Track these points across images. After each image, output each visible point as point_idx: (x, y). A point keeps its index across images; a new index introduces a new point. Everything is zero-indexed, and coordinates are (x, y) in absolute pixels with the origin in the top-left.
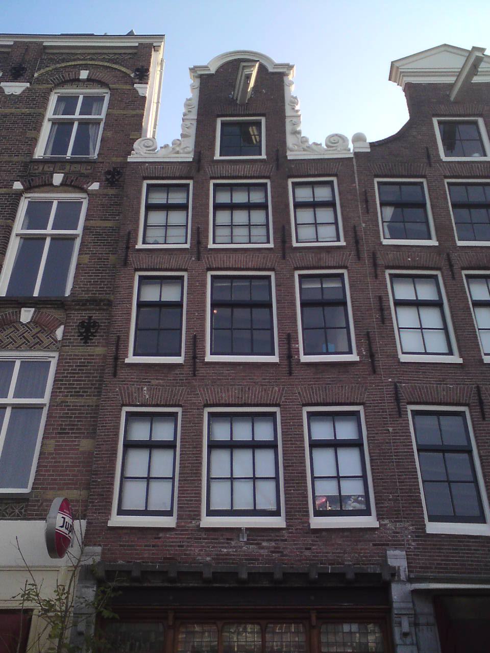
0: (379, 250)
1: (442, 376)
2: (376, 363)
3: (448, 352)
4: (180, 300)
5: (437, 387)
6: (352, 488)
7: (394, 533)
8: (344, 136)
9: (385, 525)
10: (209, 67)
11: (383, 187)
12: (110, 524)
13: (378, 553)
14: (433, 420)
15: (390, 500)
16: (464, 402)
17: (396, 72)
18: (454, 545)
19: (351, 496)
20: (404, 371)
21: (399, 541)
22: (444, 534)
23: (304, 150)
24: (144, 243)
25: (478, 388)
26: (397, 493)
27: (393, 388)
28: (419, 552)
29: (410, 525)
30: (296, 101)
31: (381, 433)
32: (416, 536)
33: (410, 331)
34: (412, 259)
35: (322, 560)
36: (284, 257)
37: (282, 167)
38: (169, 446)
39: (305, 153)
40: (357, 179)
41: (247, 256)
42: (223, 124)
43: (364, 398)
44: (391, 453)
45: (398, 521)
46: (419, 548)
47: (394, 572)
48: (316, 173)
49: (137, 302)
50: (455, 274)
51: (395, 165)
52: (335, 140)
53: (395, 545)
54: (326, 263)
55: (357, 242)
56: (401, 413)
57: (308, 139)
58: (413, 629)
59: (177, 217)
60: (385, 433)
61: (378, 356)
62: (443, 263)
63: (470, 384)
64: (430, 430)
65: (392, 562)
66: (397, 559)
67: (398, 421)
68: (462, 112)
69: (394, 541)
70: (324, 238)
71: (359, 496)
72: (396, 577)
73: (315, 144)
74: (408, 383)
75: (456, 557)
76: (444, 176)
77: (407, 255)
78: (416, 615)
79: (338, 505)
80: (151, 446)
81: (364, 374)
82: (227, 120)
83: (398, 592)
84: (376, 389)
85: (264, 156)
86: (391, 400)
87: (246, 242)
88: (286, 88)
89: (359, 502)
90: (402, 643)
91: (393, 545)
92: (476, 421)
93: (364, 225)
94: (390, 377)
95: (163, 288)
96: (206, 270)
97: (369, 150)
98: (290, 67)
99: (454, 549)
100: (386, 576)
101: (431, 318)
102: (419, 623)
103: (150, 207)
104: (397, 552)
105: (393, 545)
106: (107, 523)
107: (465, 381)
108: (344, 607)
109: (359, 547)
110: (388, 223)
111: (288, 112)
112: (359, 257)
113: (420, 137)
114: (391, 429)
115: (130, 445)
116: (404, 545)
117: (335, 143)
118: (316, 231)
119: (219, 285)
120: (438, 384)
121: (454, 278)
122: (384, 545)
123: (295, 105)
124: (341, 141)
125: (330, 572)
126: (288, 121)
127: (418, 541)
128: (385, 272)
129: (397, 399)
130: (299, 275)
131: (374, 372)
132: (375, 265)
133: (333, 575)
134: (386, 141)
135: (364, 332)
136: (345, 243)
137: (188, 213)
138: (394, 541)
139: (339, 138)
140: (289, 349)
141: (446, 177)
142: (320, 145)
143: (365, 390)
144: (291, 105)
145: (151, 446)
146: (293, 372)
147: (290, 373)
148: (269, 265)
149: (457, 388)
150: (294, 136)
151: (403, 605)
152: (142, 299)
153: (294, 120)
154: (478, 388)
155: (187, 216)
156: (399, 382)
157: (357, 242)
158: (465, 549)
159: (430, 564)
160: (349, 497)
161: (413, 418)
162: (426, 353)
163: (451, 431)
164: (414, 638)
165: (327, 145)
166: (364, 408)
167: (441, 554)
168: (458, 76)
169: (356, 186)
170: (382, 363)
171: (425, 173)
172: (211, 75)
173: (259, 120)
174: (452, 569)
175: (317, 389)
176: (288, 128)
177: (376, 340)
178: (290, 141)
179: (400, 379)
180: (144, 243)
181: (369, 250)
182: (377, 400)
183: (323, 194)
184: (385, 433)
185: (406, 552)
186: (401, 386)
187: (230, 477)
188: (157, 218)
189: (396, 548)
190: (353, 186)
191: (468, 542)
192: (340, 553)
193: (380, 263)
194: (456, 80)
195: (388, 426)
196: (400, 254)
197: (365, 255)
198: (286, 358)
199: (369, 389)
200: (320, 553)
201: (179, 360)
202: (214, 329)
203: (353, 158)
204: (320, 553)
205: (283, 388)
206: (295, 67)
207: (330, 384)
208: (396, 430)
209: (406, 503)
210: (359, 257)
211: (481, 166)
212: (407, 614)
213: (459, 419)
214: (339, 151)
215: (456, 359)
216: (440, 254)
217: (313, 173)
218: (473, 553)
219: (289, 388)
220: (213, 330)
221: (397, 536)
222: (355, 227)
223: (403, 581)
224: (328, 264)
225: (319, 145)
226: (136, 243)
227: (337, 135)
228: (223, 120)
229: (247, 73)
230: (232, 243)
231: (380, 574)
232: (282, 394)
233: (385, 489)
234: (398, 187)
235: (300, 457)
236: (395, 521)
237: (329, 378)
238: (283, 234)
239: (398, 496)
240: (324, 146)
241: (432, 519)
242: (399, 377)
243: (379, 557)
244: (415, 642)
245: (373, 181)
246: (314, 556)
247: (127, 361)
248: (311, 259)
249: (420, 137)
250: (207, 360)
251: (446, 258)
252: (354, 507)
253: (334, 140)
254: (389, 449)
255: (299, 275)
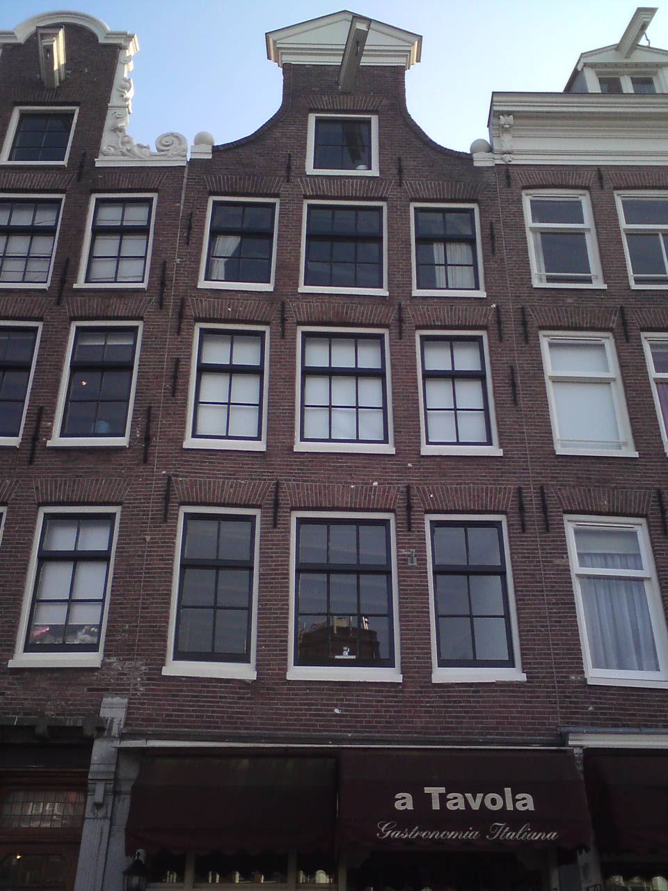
0: (191, 296)
1: (233, 467)
2: (151, 449)
3: (486, 441)
4: (380, 367)
5: (224, 482)
6: (86, 616)
7: (120, 674)
8: (207, 133)
9: (110, 664)
10: (15, 32)
11: (423, 216)
12: (12, 664)
13: (92, 701)
14: (212, 527)
15: (124, 631)
16: (379, 507)
17: (274, 45)
18: (194, 691)
19: (84, 625)
20: (185, 461)
21: (123, 685)
22: (183, 677)
23: (123, 155)
24: (87, 281)
25: (277, 484)
26: (136, 621)
27: (165, 483)
28: (147, 699)
29: (143, 665)
30: (128, 85)
31: (134, 543)
32: (148, 679)
33: (218, 407)
34: (232, 310)
35: (16, 709)
36: (58, 303)
37: (87, 177)
38: (100, 557)
39: (125, 158)
40: (183, 198)
41: (8, 300)
42: (318, 121)
43: (123, 496)
44: (142, 569)
45: (128, 660)
46: (148, 695)
47: (102, 729)
48: (130, 186)
49: (302, 367)
50: (403, 331)
51: (240, 179)
52: (170, 141)
53: (115, 690)
54: (114, 312)
55: (163, 284)
56: (167, 516)
57: (131, 139)
58: (110, 799)
59: (134, 246)
60: (140, 543)
61: (155, 441)
62: (275, 316)
63: (270, 480)
64: (454, 548)
65: (105, 713)
66: (114, 709)
67: (161, 527)
68: (350, 106)
69: (118, 685)
70: (126, 277)
71: (93, 626)
72: (106, 732)
73: (140, 146)
74: (186, 477)
75: (194, 706)
76: (303, 195)
77: (228, 303)
78: (116, 780)
79: (61, 639)
80: (76, 558)
81: (131, 464)
82: (33, 110)
83: (101, 750)
84: (142, 484)
85: (64, 163)
86: (159, 499)
87: (19, 280)
88: (119, 66)
89: (91, 634)
90: (92, 816)
91: (113, 690)
92: (655, 538)
93: (178, 260)
94: (166, 469)
95: (332, 347)
96: (414, 328)
97: (210, 157)
98: (130, 38)
99: (193, 696)
100: (88, 732)
101: (470, 394)
102: (121, 791)
103: (98, 231)
104: (117, 700)
105: (113, 690)
106: (161, 670)
107: (263, 476)
108: (31, 770)
109: (68, 693)
110: (226, 259)
111: (114, 100)
112: (161, 305)
113: (284, 140)
114: (148, 538)
115: (204, 369)
116: (129, 690)
117: (167, 146)
118: (118, 266)
119: (115, 343)
120: (227, 478)
121: (283, 336)
122: (101, 690)
123: (126, 92)
124: (176, 142)
125: (15, 724)
126: (110, 112)
127: (148, 685)
128: (193, 326)
129: (167, 498)
130: (303, 333)
131: (145, 461)
132: (181, 316)
133: (19, 727)
134: (450, 152)
135: (145, 407)
136: (388, 293)
137: (148, 239)
138: (118, 685)
139: (174, 139)
140: (38, 428)
141: (306, 197)
142: (148, 147)
143: (128, 485)
144: (120, 91)
145: (76, 558)
146: (35, 459)
147: (31, 461)
148: (36, 313)
149: (250, 484)
150: (115, 134)
151: (102, 768)
152: (204, 361)
153: (119, 112)
154: (277, 484)
155: (147, 242)
156: (174, 475)
157: (163, 284)
158: (207, 697)
159: (157, 715)
160: (81, 627)
161: (432, 532)
162: (458, 443)
163: (483, 548)
164: (109, 812)
165: (159, 150)
166: (508, 518)
167: (175, 703)
168: (344, 55)
169: (179, 207)
170: (158, 449)
171: (279, 190)
172: (17, 46)
173: (368, 118)
174: (184, 721)
175: (63, 483)
176: (109, 123)
177: (158, 418)
178: (107, 140)
179: (178, 471)
180: (87, 281)
181: (177, 296)
182: (140, 499)
183: (136, 216)
184: (140, 543)
185: (130, 699)
186: (176, 481)
187: (68, 598)
188: (107, 246)
189: (117, 694)
190: (176, 206)
191: (215, 687)
192: (41, 700)
193: (188, 313)
194: (343, 60)
195: (146, 534)
196: (218, 302)
197: (171, 303)
198: (30, 440)
199: (133, 485)
200: (15, 699)
201: (122, 441)
202: (71, 402)
203: (184, 167)
204: (15, 699)
205: (17, 481)
206: (135, 36)
207: (81, 476)
208: (155, 539)
209: (145, 636)
210: (161, 305)
211: (318, 181)
212: (103, 780)
213: (382, 529)
214: (169, 157)
215: (495, 451)
216: (273, 304)
217: (126, 187)
218: (218, 702)
219: (25, 481)
220: (69, 403)
221: (122, 679)
222: (165, 263)
223: (114, 737)
224: (118, 313)
225: (145, 147)
226: (75, 280)
227: (172, 134)
228: (23, 110)
229: (46, 44)
230: (116, 282)
231: (81, 728)
232: (14, 489)
233: (122, 617)
234: (353, 213)
235: (18, 573)
236: (124, 660)
237: (82, 468)
238: (65, 269)
239: (137, 627)
240: (154, 150)
241: (443, 663)
242: (178, 468)
243: (92, 705)
244: (109, 815)
245: (409, 207)
246: (6, 704)
247: (49, 444)
248: (95, 305)
249: (284, 140)
250: (186, 445)
251: (280, 309)
252: (83, 641)
253: (167, 142)
254: (139, 565)
255: (421, 337)
